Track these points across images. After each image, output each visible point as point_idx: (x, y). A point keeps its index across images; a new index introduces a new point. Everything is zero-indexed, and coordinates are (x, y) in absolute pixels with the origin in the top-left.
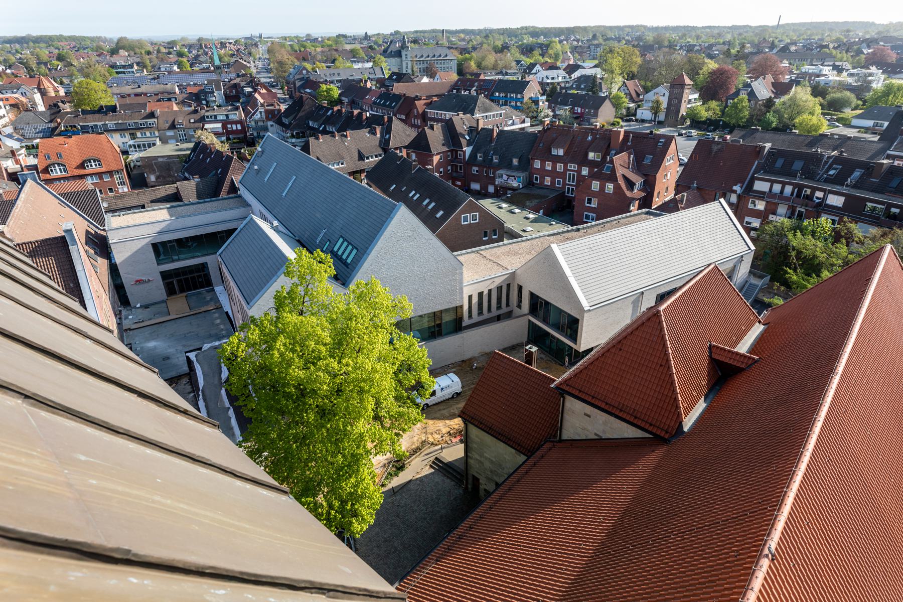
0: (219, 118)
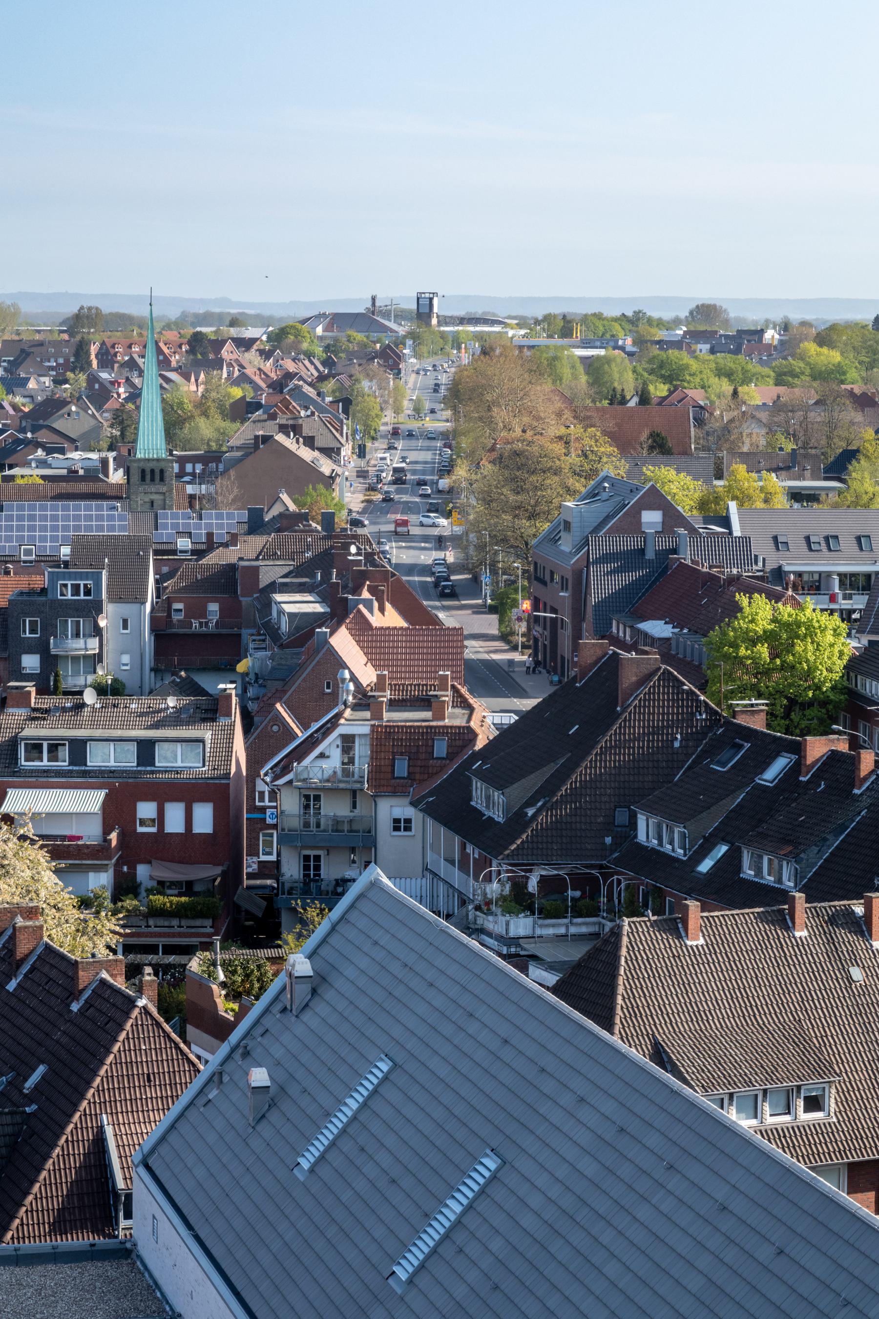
0: (100, 757)
